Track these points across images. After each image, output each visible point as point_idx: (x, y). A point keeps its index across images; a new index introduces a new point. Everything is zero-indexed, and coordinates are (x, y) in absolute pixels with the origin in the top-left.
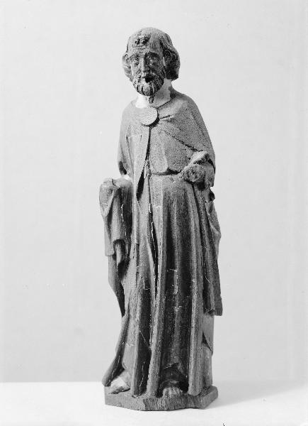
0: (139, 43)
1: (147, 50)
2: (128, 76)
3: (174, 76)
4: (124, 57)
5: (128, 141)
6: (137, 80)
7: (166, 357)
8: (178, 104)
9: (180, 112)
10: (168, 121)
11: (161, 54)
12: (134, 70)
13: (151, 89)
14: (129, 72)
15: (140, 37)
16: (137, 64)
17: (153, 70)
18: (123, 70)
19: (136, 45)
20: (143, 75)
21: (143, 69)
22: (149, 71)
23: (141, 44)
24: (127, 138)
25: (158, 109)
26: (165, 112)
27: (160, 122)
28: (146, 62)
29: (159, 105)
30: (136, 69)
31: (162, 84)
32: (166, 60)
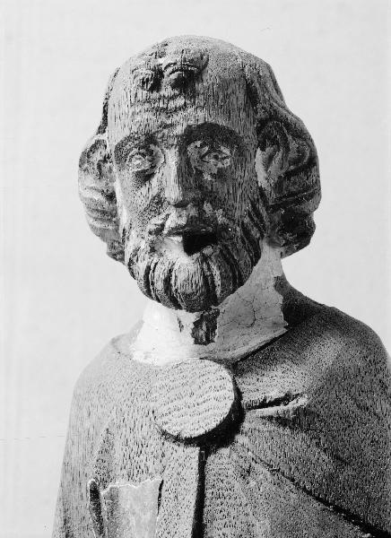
0: (156, 86)
1: (196, 115)
2: (102, 234)
3: (297, 232)
4: (87, 155)
5: (97, 509)
6: (144, 245)
7: (224, 256)
8: (328, 351)
9: (333, 380)
10: (281, 421)
11: (249, 135)
12: (129, 201)
13: (208, 282)
14: (106, 212)
15: (163, 61)
16: (145, 177)
17: (217, 202)
18: (81, 210)
19: (142, 94)
20: (174, 219)
21: (173, 193)
22: (198, 204)
23: (167, 91)
24: (95, 493)
25: (237, 367)
26: (271, 383)
27: (246, 425)
28: (188, 174)
29: (242, 350)
30: (145, 194)
31: (254, 263)
32: (268, 162)
